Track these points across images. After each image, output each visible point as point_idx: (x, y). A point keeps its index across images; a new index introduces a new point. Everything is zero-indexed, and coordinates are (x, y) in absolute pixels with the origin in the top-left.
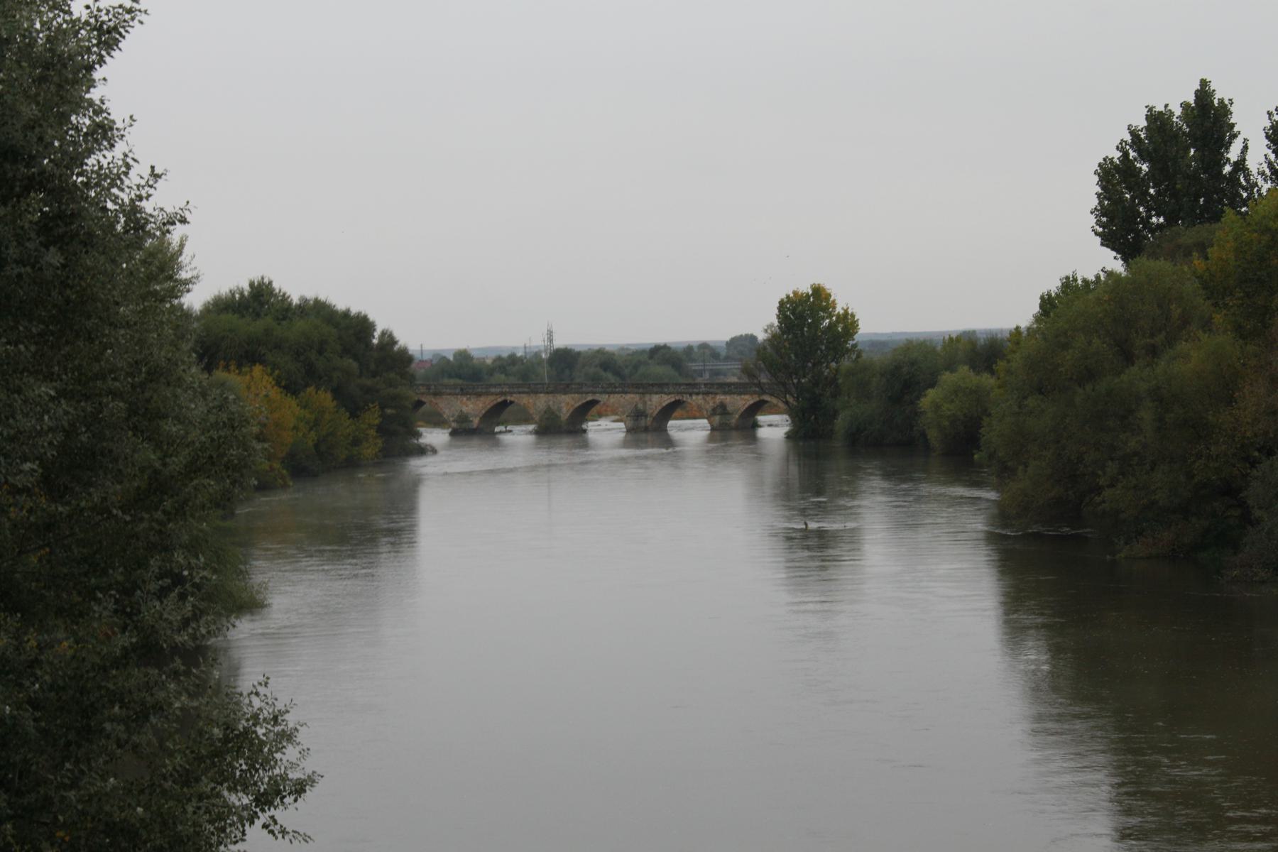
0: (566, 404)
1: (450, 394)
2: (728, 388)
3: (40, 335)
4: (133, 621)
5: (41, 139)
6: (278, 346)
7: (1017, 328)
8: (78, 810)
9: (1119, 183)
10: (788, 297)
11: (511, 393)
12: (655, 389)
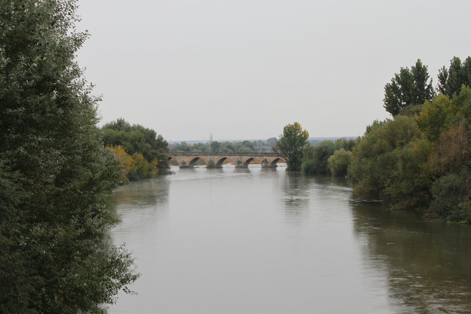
0: (216, 159)
1: (180, 155)
2: (267, 154)
3: (56, 135)
4: (84, 225)
5: (57, 74)
6: (126, 140)
7: (359, 137)
8: (66, 284)
9: (392, 91)
10: (287, 126)
11: (199, 155)
12: (245, 154)
